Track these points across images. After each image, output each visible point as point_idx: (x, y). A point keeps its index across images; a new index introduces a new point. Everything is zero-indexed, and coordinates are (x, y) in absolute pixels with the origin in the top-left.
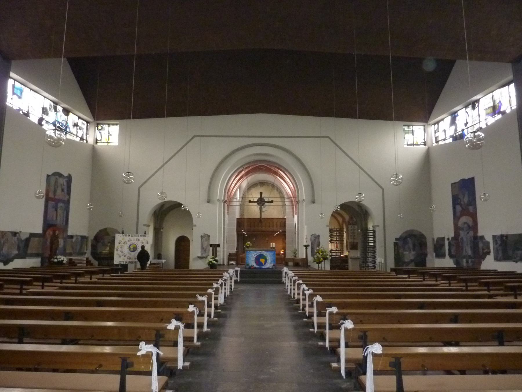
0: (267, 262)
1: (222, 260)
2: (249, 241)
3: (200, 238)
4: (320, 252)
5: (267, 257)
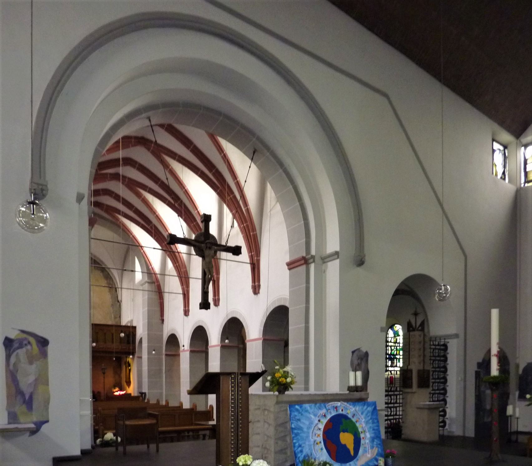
5: (357, 425)
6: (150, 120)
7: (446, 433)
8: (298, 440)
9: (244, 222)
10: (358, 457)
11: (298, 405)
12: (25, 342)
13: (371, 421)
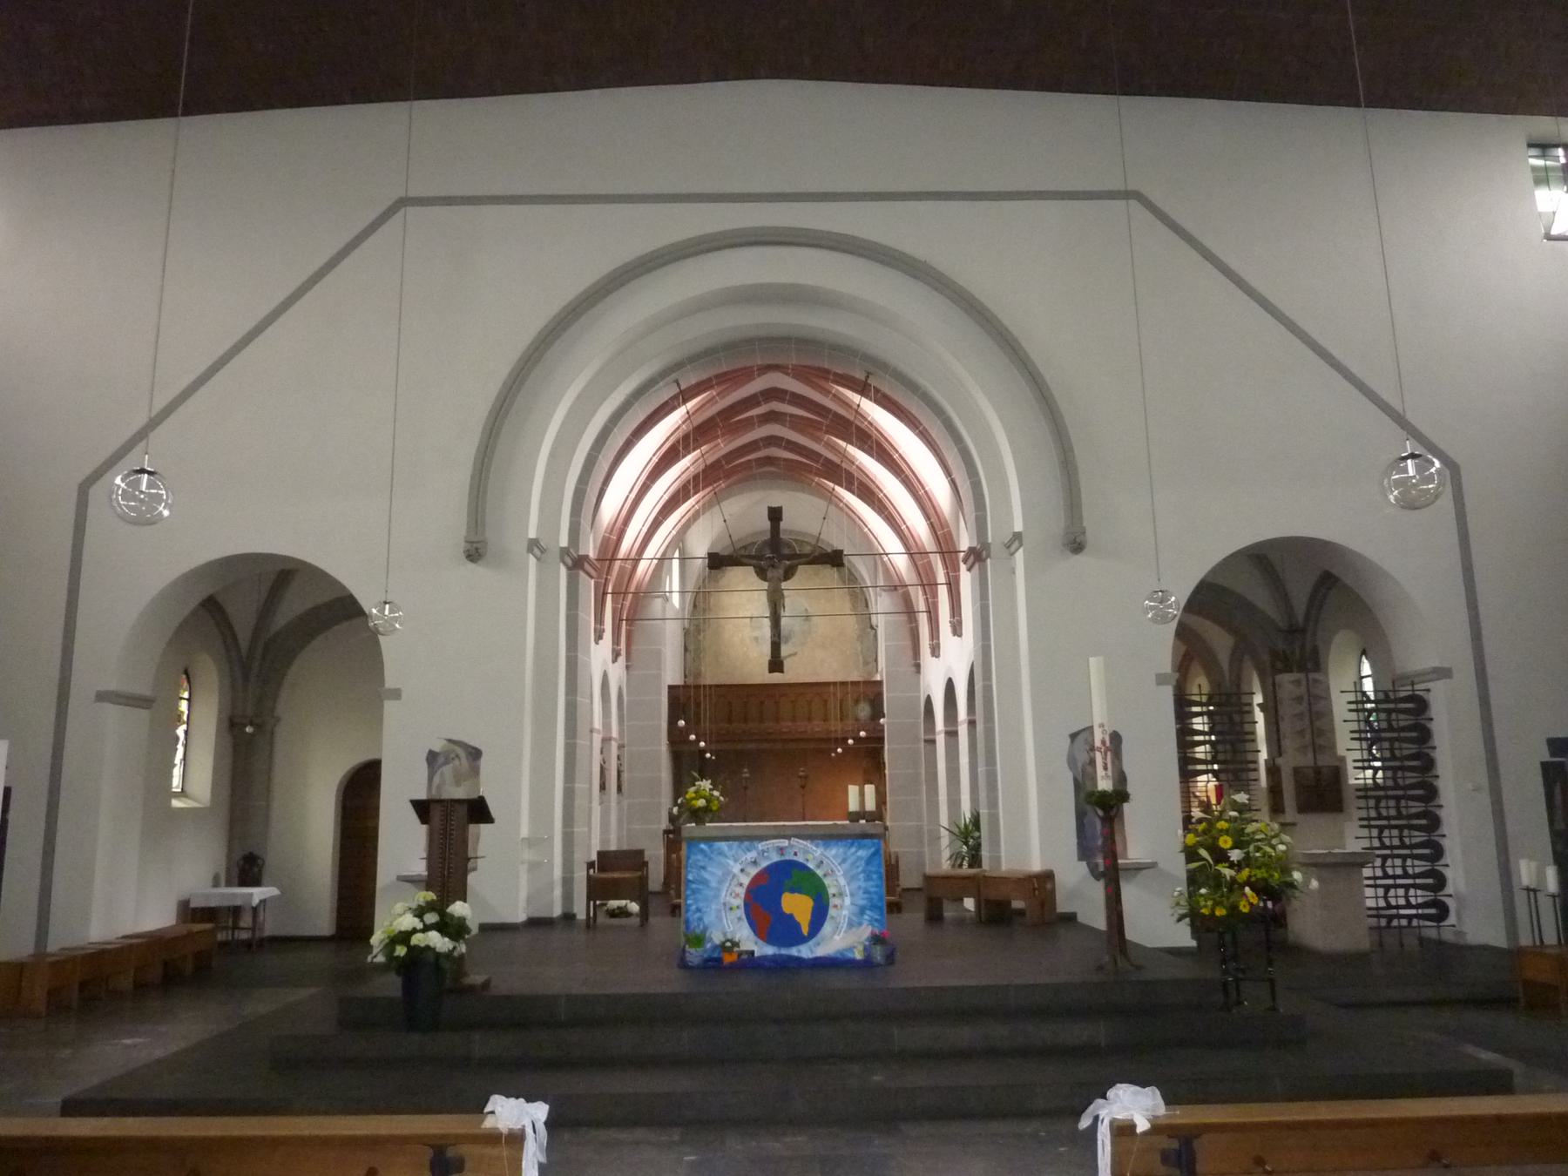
0: (832, 912)
1: (558, 892)
2: (703, 777)
3: (425, 765)
4: (1225, 842)
5: (827, 881)
6: (678, 385)
7: (1447, 935)
8: (696, 900)
10: (819, 936)
11: (705, 843)
12: (452, 755)
13: (862, 875)
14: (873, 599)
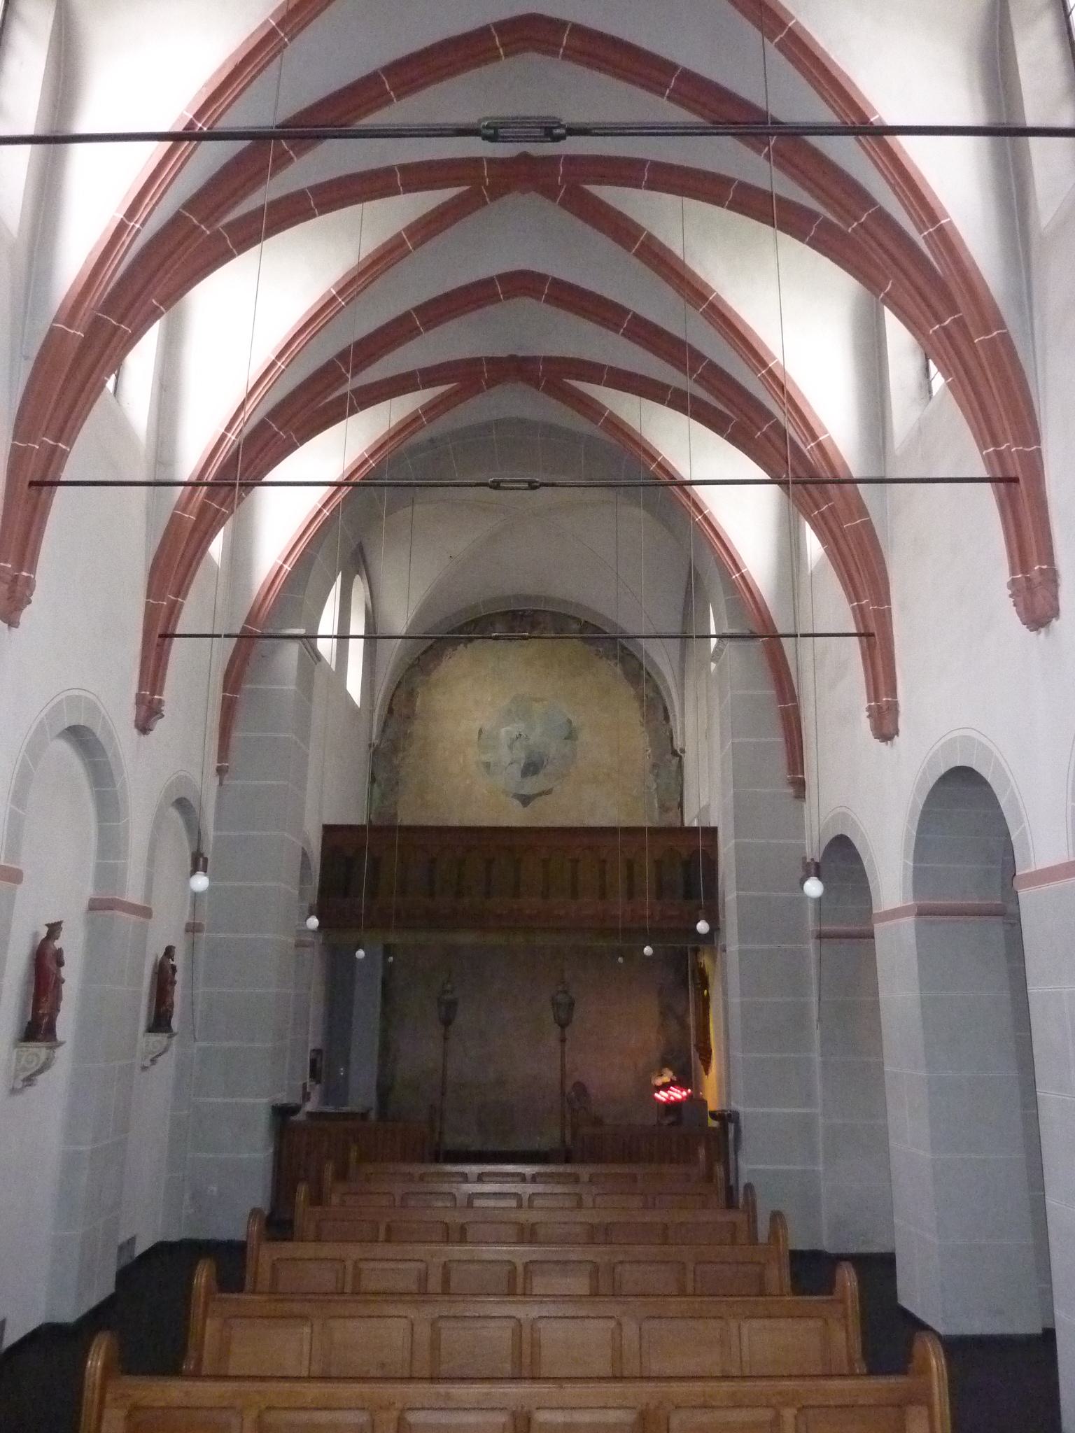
9: (940, 307)
14: (677, 708)
